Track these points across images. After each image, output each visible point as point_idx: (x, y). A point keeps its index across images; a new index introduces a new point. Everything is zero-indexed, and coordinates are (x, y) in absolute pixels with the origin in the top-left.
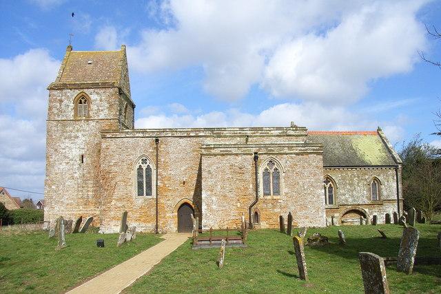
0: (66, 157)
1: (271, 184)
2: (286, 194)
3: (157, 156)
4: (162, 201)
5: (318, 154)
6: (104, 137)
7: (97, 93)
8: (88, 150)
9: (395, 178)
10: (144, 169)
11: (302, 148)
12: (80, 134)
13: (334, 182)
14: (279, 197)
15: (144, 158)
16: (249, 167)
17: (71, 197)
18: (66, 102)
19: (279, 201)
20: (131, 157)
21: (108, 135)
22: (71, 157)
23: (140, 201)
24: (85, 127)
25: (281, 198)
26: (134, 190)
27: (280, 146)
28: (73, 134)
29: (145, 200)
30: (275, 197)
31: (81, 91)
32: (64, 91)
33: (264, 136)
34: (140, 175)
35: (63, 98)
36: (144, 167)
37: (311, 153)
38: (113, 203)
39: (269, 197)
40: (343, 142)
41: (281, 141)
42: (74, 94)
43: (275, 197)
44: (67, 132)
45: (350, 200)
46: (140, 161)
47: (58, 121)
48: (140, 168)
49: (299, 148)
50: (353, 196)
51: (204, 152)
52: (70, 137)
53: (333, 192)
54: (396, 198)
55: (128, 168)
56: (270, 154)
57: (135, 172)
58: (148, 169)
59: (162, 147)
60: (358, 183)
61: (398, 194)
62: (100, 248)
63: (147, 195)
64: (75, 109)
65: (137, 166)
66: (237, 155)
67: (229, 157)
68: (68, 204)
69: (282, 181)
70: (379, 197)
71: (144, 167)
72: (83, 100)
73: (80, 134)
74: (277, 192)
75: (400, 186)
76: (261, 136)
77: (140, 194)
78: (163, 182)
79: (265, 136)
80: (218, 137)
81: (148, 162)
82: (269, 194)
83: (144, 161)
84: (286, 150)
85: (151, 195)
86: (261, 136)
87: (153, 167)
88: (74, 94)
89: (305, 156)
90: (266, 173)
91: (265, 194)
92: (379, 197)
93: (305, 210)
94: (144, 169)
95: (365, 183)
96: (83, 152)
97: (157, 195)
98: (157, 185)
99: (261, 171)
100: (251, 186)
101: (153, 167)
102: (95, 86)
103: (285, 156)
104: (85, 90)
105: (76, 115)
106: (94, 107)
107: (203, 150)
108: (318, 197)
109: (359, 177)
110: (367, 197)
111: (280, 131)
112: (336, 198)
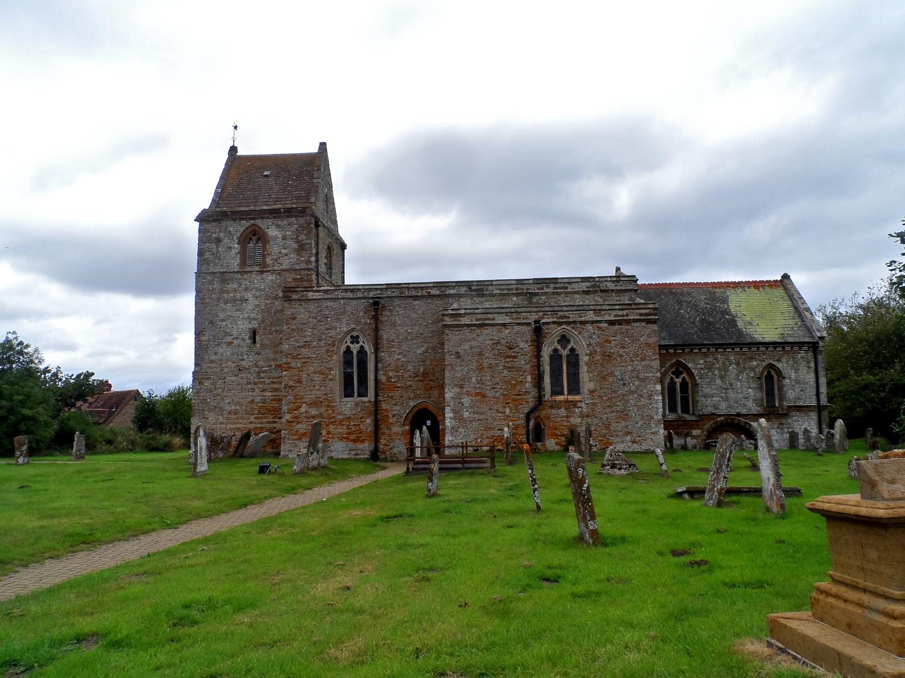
0: (227, 334)
1: (565, 375)
2: (592, 392)
3: (376, 330)
4: (384, 406)
5: (649, 322)
6: (287, 299)
7: (278, 226)
8: (263, 322)
9: (812, 365)
10: (355, 352)
11: (621, 313)
12: (249, 295)
13: (691, 374)
14: (577, 398)
15: (355, 334)
16: (525, 346)
17: (236, 400)
18: (226, 241)
19: (579, 404)
20: (333, 333)
21: (294, 297)
22: (235, 333)
23: (347, 406)
24: (256, 278)
25: (583, 398)
26: (336, 386)
27: (582, 309)
28: (238, 295)
29: (357, 405)
30: (571, 398)
31: (253, 222)
32: (224, 224)
33: (559, 294)
34: (348, 363)
35: (222, 235)
36: (355, 348)
37: (635, 321)
38: (303, 410)
39: (560, 398)
40: (713, 298)
41: (588, 300)
42: (238, 228)
43: (571, 398)
44: (228, 292)
45: (723, 405)
46: (348, 339)
47: (215, 273)
48: (348, 351)
49: (615, 313)
50: (726, 399)
51: (448, 321)
52: (234, 301)
53: (690, 391)
54: (814, 403)
55: (328, 351)
56: (560, 324)
57: (336, 361)
58: (362, 352)
59: (385, 317)
60: (738, 375)
61: (818, 395)
62: (257, 468)
63: (359, 396)
64: (243, 253)
65: (343, 348)
66: (504, 325)
67: (490, 328)
68: (230, 413)
69: (583, 369)
70: (781, 400)
71: (355, 348)
72: (255, 236)
73: (249, 295)
74: (575, 388)
75: (823, 381)
76: (554, 293)
77: (348, 394)
78: (386, 374)
79: (562, 293)
80: (478, 295)
81: (361, 339)
82: (562, 393)
83: (355, 340)
84: (591, 316)
85: (366, 396)
86: (554, 293)
87: (369, 349)
88: (238, 228)
89: (624, 327)
90: (555, 357)
91: (554, 393)
92: (781, 400)
93: (626, 420)
94: (355, 352)
95: (752, 375)
96: (255, 325)
97: (377, 395)
98: (376, 380)
99: (546, 352)
100: (529, 378)
101: (369, 349)
102: (275, 213)
103: (589, 327)
104: (259, 222)
105: (243, 263)
106: (274, 249)
107: (447, 319)
108: (650, 397)
109: (738, 364)
110: (754, 400)
111: (588, 284)
112: (695, 402)
